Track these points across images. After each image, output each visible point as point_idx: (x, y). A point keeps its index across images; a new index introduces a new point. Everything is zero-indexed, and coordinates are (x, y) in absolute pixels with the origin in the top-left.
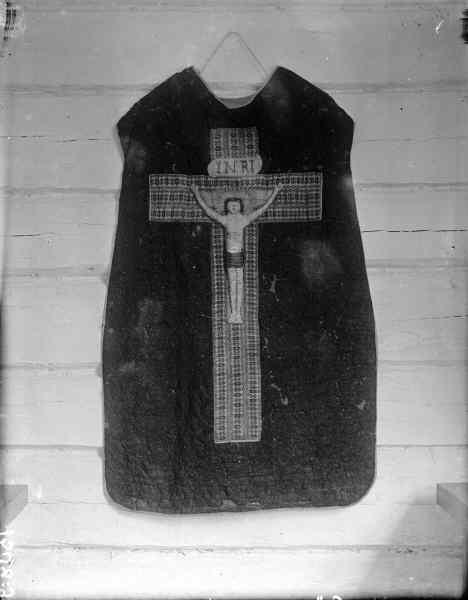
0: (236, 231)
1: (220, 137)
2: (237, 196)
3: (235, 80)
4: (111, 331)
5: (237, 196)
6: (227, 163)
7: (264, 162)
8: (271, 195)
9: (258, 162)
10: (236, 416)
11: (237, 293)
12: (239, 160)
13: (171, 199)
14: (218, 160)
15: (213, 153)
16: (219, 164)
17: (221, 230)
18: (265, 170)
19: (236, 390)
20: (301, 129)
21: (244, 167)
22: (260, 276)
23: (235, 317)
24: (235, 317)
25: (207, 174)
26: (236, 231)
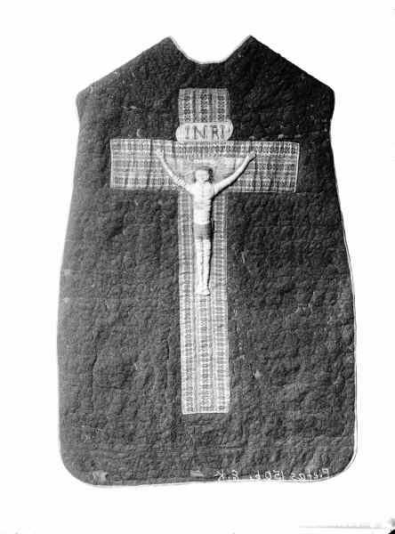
0: (198, 198)
1: (187, 99)
2: (202, 165)
3: (210, 45)
4: (66, 300)
5: (202, 165)
6: (195, 128)
7: (235, 129)
8: (241, 163)
9: (228, 127)
10: (208, 387)
11: (202, 273)
12: (209, 124)
13: (135, 162)
14: (187, 124)
15: (182, 117)
16: (188, 129)
17: (189, 198)
18: (238, 136)
19: (207, 370)
20: (119, 421)
21: (215, 132)
22: (229, 248)
23: (201, 288)
24: (201, 288)
25: (174, 139)
26: (198, 198)
